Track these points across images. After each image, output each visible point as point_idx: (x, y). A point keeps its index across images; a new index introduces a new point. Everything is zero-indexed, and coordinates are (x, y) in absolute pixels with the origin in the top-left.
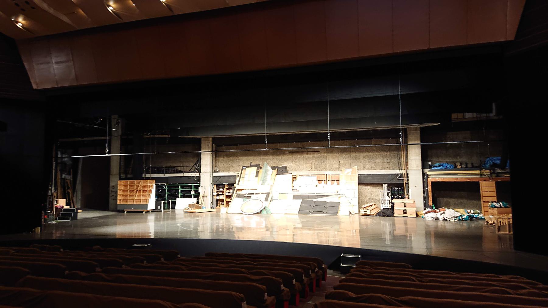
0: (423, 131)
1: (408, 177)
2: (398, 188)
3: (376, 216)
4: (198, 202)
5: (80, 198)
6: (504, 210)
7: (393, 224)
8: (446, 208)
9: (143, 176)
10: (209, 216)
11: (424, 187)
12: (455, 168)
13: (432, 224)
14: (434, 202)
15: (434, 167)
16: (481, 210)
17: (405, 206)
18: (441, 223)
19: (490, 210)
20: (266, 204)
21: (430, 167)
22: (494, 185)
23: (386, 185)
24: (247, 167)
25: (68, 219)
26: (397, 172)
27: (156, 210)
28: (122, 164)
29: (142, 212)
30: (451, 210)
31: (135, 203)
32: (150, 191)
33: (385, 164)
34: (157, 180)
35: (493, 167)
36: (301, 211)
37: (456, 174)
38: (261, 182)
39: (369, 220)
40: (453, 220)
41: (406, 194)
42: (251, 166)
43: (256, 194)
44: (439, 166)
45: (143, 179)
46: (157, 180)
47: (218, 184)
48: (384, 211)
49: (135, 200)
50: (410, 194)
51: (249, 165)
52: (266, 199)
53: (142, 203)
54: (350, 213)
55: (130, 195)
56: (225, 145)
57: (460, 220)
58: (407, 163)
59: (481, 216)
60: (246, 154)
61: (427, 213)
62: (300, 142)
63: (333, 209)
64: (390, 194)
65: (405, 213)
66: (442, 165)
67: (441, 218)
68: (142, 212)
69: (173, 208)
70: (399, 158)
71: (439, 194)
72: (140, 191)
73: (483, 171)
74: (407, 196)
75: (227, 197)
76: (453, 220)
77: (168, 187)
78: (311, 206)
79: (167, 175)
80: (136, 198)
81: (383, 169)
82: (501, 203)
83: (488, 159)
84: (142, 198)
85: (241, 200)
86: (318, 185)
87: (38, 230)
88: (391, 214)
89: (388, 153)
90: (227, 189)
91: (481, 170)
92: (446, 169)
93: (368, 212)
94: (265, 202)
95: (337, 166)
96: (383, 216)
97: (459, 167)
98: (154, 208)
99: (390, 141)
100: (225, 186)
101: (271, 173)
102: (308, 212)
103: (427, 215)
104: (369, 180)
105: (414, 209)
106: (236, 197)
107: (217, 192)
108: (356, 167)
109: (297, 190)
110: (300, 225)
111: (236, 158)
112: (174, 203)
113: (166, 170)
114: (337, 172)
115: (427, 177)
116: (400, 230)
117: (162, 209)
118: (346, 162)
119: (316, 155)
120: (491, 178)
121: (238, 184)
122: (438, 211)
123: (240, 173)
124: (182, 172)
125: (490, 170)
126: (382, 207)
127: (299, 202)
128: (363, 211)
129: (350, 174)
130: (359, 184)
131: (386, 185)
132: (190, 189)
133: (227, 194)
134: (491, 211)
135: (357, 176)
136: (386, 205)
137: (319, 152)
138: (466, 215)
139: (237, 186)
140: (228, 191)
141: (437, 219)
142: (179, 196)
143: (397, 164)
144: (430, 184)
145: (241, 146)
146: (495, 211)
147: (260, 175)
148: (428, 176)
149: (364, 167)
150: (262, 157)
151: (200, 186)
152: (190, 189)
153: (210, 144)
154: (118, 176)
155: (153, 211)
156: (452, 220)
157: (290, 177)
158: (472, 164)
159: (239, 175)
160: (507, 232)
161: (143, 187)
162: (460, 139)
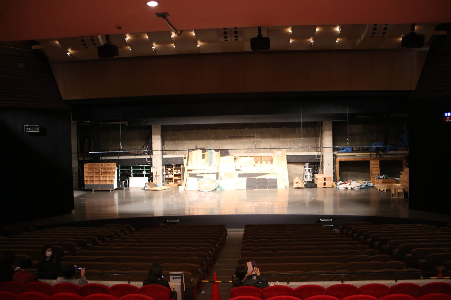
2: (316, 165)
6: (385, 180)
12: (353, 151)
13: (343, 192)
15: (340, 150)
19: (376, 180)
23: (308, 164)
26: (315, 153)
27: (119, 188)
28: (79, 148)
29: (109, 191)
30: (355, 182)
31: (101, 183)
32: (114, 172)
36: (248, 187)
37: (355, 155)
38: (208, 163)
39: (300, 191)
42: (196, 149)
43: (207, 174)
44: (343, 149)
47: (167, 164)
49: (101, 181)
52: (217, 178)
53: (108, 183)
57: (361, 188)
59: (371, 185)
61: (340, 184)
63: (273, 184)
65: (325, 184)
67: (349, 188)
68: (109, 191)
70: (317, 142)
71: (345, 170)
73: (372, 153)
75: (175, 175)
78: (256, 183)
84: (108, 179)
87: (74, 212)
89: (308, 139)
90: (175, 169)
91: (370, 152)
93: (300, 186)
96: (310, 188)
97: (355, 149)
99: (313, 131)
101: (216, 155)
103: (339, 186)
104: (294, 160)
111: (181, 142)
114: (270, 154)
115: (336, 157)
116: (319, 199)
117: (124, 187)
119: (252, 140)
121: (187, 165)
123: (187, 155)
125: (376, 153)
127: (245, 179)
130: (288, 163)
132: (143, 169)
133: (175, 173)
134: (377, 181)
140: (176, 171)
141: (347, 188)
142: (132, 175)
144: (338, 162)
147: (206, 156)
150: (205, 142)
151: (152, 167)
152: (143, 169)
155: (116, 189)
157: (232, 158)
161: (108, 169)
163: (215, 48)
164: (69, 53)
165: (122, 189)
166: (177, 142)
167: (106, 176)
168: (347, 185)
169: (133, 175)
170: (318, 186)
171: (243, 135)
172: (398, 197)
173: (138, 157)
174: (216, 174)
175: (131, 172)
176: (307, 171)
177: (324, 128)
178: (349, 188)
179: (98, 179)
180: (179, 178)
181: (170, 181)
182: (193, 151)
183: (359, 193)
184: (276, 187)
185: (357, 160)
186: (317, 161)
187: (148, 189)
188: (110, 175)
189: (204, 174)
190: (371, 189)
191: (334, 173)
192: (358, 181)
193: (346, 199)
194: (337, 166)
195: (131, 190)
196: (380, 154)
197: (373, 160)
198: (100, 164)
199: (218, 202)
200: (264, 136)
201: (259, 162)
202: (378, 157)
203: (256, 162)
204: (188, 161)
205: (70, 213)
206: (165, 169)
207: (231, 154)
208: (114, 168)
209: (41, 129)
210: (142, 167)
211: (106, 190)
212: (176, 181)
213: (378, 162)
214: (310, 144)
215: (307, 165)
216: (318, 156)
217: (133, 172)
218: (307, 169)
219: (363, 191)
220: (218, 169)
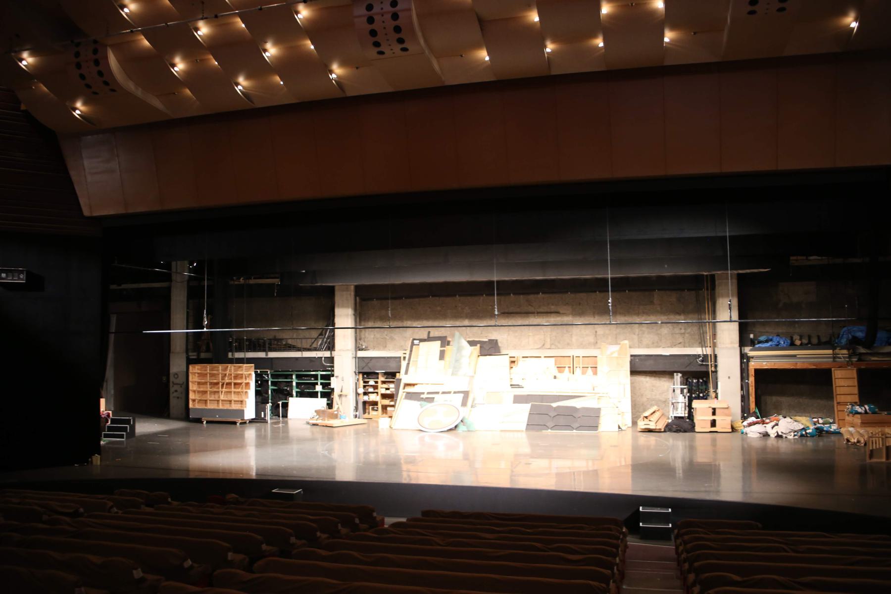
0: (740, 278)
1: (716, 361)
2: (699, 379)
3: (665, 431)
4: (330, 405)
5: (112, 392)
6: (870, 417)
7: (692, 448)
8: (781, 417)
9: (230, 355)
10: (352, 432)
11: (742, 379)
12: (792, 345)
13: (758, 444)
14: (758, 404)
15: (760, 342)
16: (834, 419)
17: (714, 413)
18: (772, 442)
19: (847, 418)
20: (464, 412)
21: (752, 343)
22: (855, 376)
23: (680, 375)
24: (421, 340)
25: (122, 436)
26: (698, 351)
27: (258, 419)
30: (788, 419)
31: (221, 407)
32: (248, 384)
33: (677, 336)
35: (853, 343)
36: (531, 426)
37: (794, 356)
39: (652, 439)
40: (791, 437)
41: (711, 390)
42: (430, 339)
43: (444, 393)
44: (767, 341)
45: (231, 361)
47: (366, 372)
48: (677, 422)
50: (719, 391)
51: (425, 337)
52: (464, 404)
53: (234, 407)
54: (619, 427)
56: (377, 299)
57: (802, 436)
58: (714, 335)
59: (834, 427)
60: (418, 317)
61: (750, 425)
62: (523, 294)
63: (589, 420)
64: (685, 391)
66: (771, 340)
67: (773, 433)
68: (235, 423)
69: (285, 416)
70: (701, 324)
71: (768, 391)
72: (229, 384)
73: (837, 351)
74: (713, 395)
75: (384, 396)
76: (791, 437)
77: (273, 376)
78: (553, 417)
79: (272, 355)
80: (222, 397)
81: (673, 345)
82: (867, 407)
83: (845, 329)
84: (234, 397)
85: (414, 404)
86: (558, 375)
87: (97, 459)
88: (690, 427)
90: (384, 382)
91: (834, 348)
92: (777, 347)
93: (652, 426)
94: (462, 409)
95: (591, 339)
96: (677, 431)
97: (798, 342)
98: (254, 416)
99: (688, 297)
100: (380, 376)
102: (546, 427)
103: (747, 430)
104: (649, 366)
105: (729, 419)
106: (406, 398)
107: (364, 387)
108: (626, 342)
109: (518, 386)
110: (527, 450)
112: (285, 406)
113: (270, 344)
115: (748, 361)
116: (702, 457)
118: (607, 332)
120: (849, 364)
121: (406, 373)
122: (768, 421)
123: (408, 352)
124: (299, 350)
125: (848, 349)
126: (673, 414)
127: (527, 407)
128: (642, 424)
129: (616, 355)
130: (633, 372)
131: (680, 375)
132: (315, 381)
133: (384, 391)
134: (849, 419)
135: (628, 359)
136: (679, 410)
137: (558, 313)
138: (812, 427)
139: (401, 376)
140: (385, 386)
141: (766, 435)
142: (294, 394)
143: (697, 337)
144: (752, 372)
145: (408, 300)
146: (857, 420)
147: (448, 356)
148: (749, 359)
149: (640, 342)
151: (333, 376)
152: (315, 381)
153: (350, 295)
154: (184, 356)
155: (252, 421)
156: (791, 437)
157: (505, 360)
158: (819, 337)
159: (407, 356)
160: (884, 460)
161: (236, 377)
162: (798, 292)
163: (375, 83)
164: (78, 112)
165: (264, 421)
167: (231, 392)
168: (768, 428)
169: (297, 392)
170: (697, 429)
171: (531, 309)
172: (887, 458)
173: (307, 354)
174: (462, 395)
175: (291, 386)
176: (678, 391)
177: (718, 290)
178: (773, 433)
179: (216, 397)
180: (392, 403)
181: (373, 409)
182: (422, 344)
183: (799, 447)
184: (595, 427)
185: (799, 366)
186: (703, 369)
187: (315, 422)
188: (239, 390)
189: (438, 393)
190: (833, 438)
191: (744, 399)
192: (798, 418)
193: (767, 463)
194: (751, 380)
195: (290, 422)
196: (861, 354)
197: (841, 367)
199: (466, 457)
200: (579, 311)
201: (567, 369)
202: (855, 360)
203: (560, 369)
204: (408, 364)
205: (88, 462)
207: (503, 352)
209: (29, 275)
210: (316, 377)
211: (229, 422)
212: (385, 408)
213: (855, 372)
214: (689, 330)
215: (678, 377)
216: (705, 357)
217: (297, 387)
218: (678, 387)
219: (810, 443)
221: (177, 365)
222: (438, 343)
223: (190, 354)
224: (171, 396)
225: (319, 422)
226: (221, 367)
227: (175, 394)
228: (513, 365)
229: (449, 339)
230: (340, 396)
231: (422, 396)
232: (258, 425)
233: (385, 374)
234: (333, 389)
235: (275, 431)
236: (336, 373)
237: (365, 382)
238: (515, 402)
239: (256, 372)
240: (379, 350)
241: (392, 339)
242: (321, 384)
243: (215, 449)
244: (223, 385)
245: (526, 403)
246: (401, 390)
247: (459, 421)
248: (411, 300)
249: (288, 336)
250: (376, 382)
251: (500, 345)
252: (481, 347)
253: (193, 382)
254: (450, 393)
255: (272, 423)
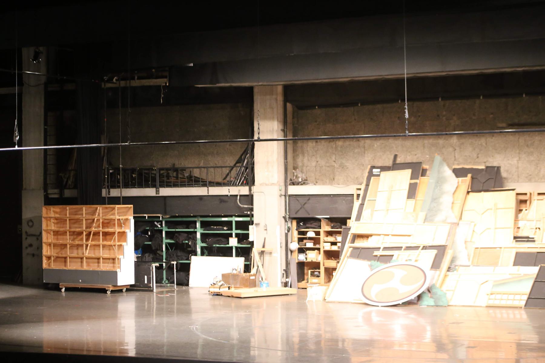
9: (104, 193)
24: (384, 169)
31: (85, 267)
32: (123, 235)
34: (139, 204)
42: (396, 166)
43: (408, 248)
45: (102, 201)
46: (139, 204)
47: (302, 218)
51: (389, 163)
52: (436, 265)
53: (104, 267)
55: (72, 246)
56: (320, 107)
68: (104, 291)
72: (96, 234)
79: (165, 192)
84: (102, 253)
85: (363, 265)
90: (329, 233)
94: (430, 273)
100: (323, 223)
106: (352, 256)
107: (300, 240)
111: (354, 143)
112: (185, 269)
113: (161, 176)
121: (358, 218)
123: (363, 187)
124: (205, 184)
132: (227, 232)
133: (328, 247)
140: (331, 239)
142: (199, 250)
145: (367, 107)
147: (421, 193)
151: (252, 223)
154: (42, 194)
155: (131, 289)
159: (361, 193)
166: (340, 143)
169: (202, 248)
173: (215, 191)
174: (435, 252)
175: (195, 239)
181: (313, 274)
182: (383, 174)
187: (217, 290)
188: (112, 243)
189: (400, 248)
198: (100, 209)
204: (362, 205)
206: (295, 233)
208: (126, 220)
210: (229, 224)
211: (96, 289)
217: (167, 238)
220: (451, 234)
221: (32, 205)
222: (408, 172)
223: (50, 191)
224: (25, 252)
225: (224, 290)
226: (84, 209)
227: (29, 250)
228: (523, 207)
229: (425, 166)
230: (262, 253)
231: (376, 253)
232: (137, 294)
233: (331, 220)
234: (252, 243)
235: (160, 301)
236: (256, 220)
237: (300, 233)
238: (517, 263)
239: (134, 217)
240: (324, 183)
241: (343, 167)
242: (237, 235)
243: (39, 320)
244: (88, 235)
245: (535, 265)
246: (348, 245)
247: (424, 289)
248: (371, 107)
249: (190, 163)
250: (318, 233)
251: (504, 174)
252: (472, 178)
253: (48, 232)
254: (417, 248)
255: (158, 293)
